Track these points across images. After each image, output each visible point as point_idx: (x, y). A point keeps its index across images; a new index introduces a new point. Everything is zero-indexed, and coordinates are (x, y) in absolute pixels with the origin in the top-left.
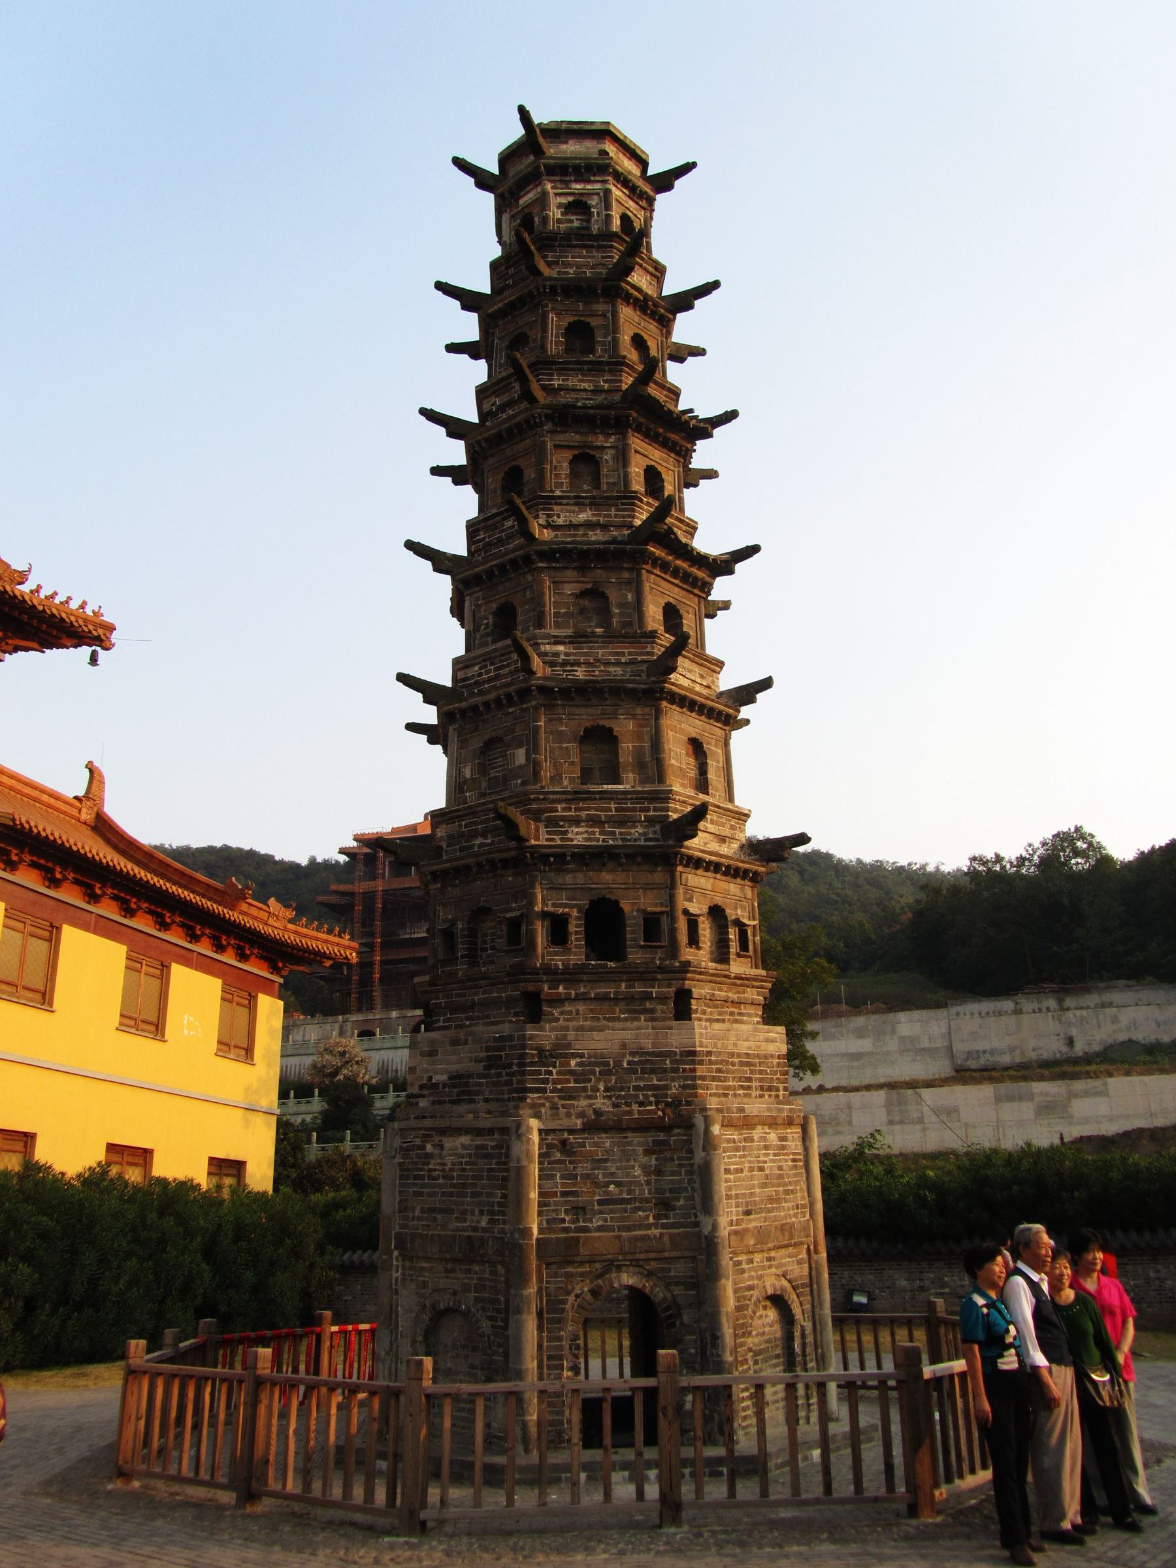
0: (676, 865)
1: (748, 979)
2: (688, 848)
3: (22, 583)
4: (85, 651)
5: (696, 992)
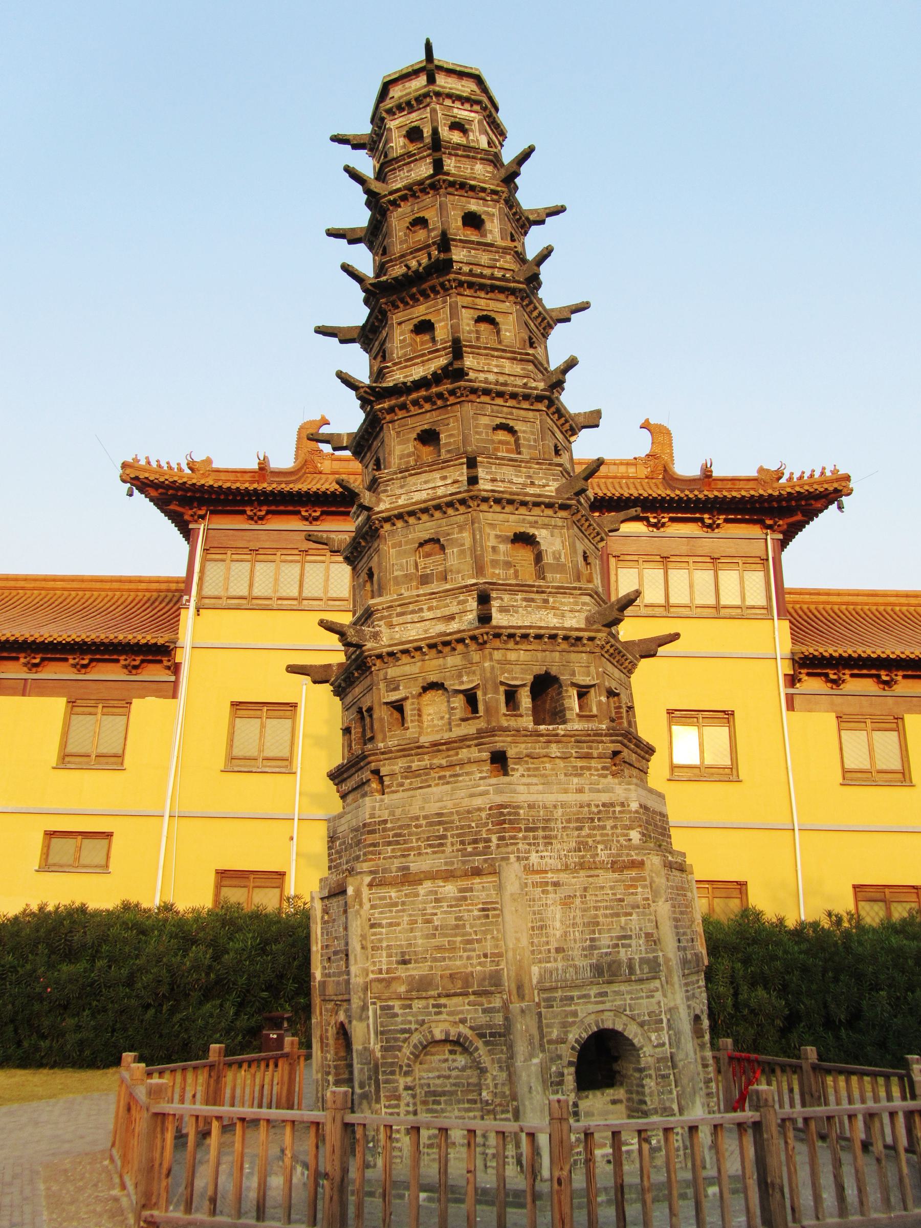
0: (370, 667)
1: (455, 742)
2: (369, 650)
3: (780, 478)
4: (833, 507)
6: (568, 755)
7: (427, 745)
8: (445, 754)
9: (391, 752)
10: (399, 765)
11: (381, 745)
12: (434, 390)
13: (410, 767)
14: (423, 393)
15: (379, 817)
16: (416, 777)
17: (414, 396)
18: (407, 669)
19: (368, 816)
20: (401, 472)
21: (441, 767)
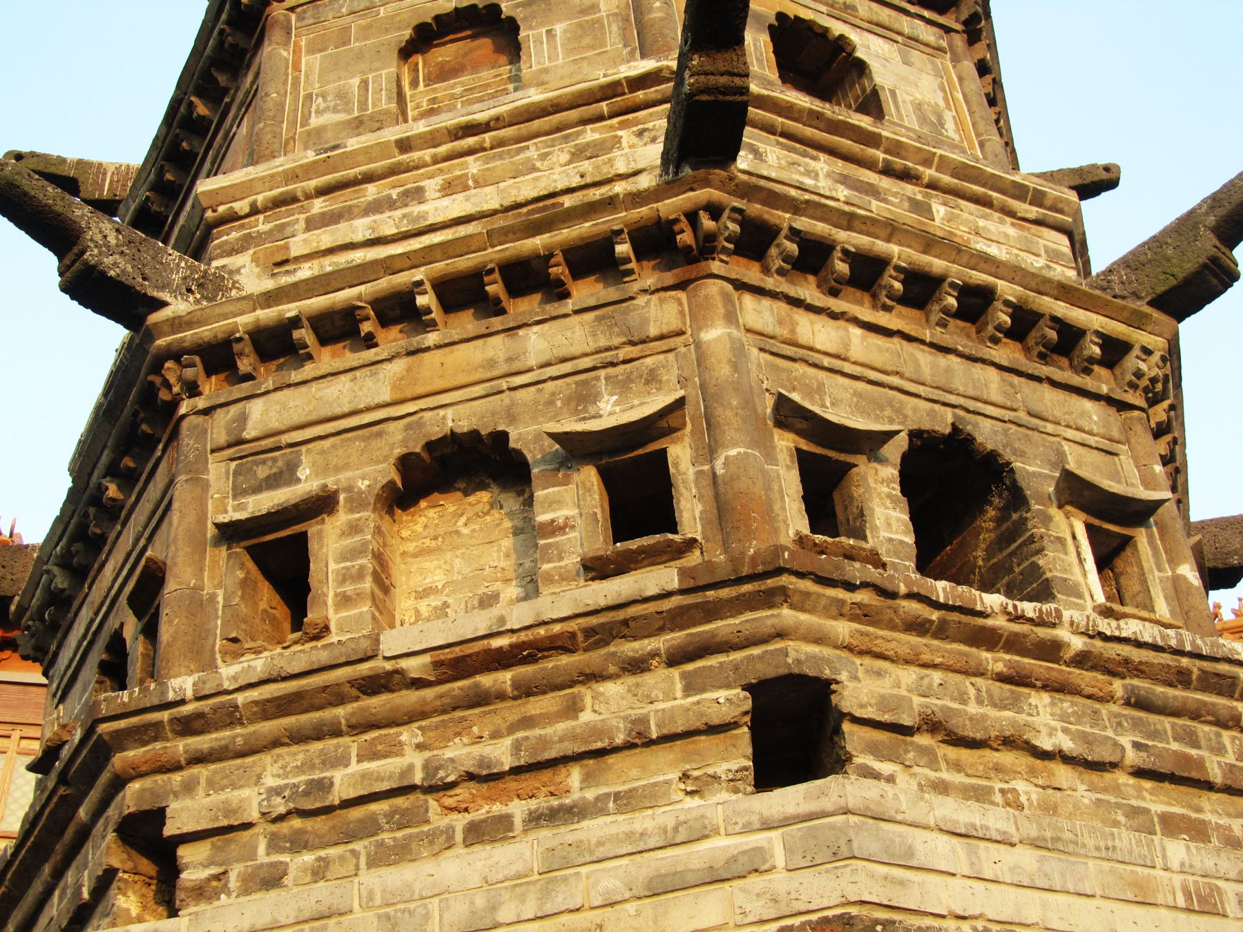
0: (175, 403)
2: (177, 324)
6: (1106, 755)
7: (414, 666)
8: (509, 712)
11: (183, 684)
16: (350, 836)
18: (338, 394)
21: (484, 777)
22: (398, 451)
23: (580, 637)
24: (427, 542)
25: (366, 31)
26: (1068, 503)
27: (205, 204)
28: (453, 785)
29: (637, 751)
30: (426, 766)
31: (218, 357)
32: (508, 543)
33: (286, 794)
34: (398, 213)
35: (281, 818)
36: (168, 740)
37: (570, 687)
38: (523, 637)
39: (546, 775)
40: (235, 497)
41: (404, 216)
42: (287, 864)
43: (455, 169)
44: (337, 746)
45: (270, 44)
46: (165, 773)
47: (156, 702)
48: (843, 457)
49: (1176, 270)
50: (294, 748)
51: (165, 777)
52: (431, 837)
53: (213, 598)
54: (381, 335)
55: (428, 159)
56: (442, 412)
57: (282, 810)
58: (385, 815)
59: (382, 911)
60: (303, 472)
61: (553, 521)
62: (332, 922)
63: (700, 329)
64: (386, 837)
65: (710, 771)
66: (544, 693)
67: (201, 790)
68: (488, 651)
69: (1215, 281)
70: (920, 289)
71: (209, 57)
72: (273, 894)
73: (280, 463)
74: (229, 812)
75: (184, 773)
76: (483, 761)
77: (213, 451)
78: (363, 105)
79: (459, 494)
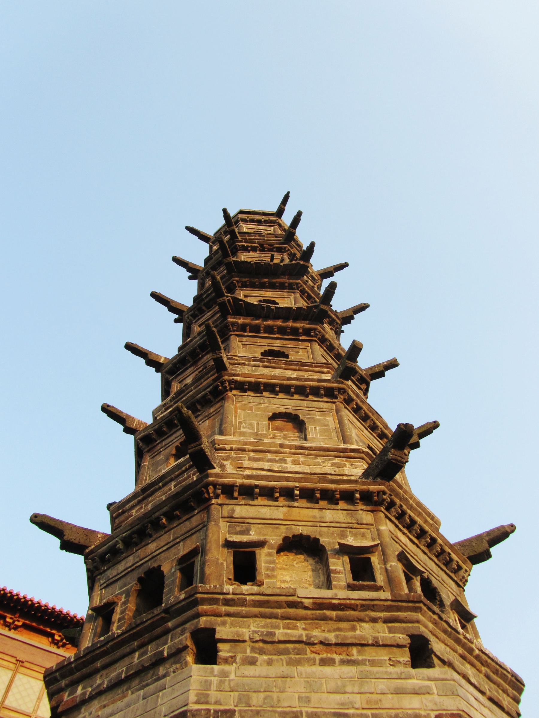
0: (210, 499)
2: (217, 475)
5: (222, 632)
7: (307, 602)
9: (243, 603)
10: (250, 629)
12: (291, 324)
13: (273, 634)
14: (279, 323)
15: (217, 702)
17: (270, 322)
19: (192, 697)
20: (254, 361)
22: (284, 535)
23: (359, 606)
24: (284, 566)
25: (258, 409)
26: (455, 610)
27: (216, 442)
28: (315, 644)
29: (374, 647)
30: (307, 636)
31: (228, 490)
32: (310, 573)
33: (259, 633)
34: (278, 465)
35: (257, 641)
36: (219, 605)
37: (353, 621)
38: (342, 601)
39: (345, 648)
40: (229, 534)
41: (280, 466)
42: (258, 658)
43: (296, 457)
44: (276, 622)
45: (228, 403)
46: (215, 616)
47: (219, 591)
48: (411, 575)
49: (476, 550)
50: (261, 619)
51: (215, 618)
52: (309, 660)
53: (222, 564)
54: (281, 499)
55: (288, 452)
56: (298, 527)
57: (258, 638)
58: (292, 649)
59: (306, 679)
60: (252, 532)
61: (335, 570)
62: (288, 679)
63: (379, 525)
64: (292, 656)
65: (398, 659)
66: (345, 621)
67: (228, 626)
68: (331, 603)
69: (486, 556)
70: (422, 534)
71: (197, 399)
72: (253, 667)
73: (244, 528)
74: (238, 635)
75: (222, 618)
76: (326, 639)
77: (222, 517)
78: (258, 430)
79: (294, 554)
